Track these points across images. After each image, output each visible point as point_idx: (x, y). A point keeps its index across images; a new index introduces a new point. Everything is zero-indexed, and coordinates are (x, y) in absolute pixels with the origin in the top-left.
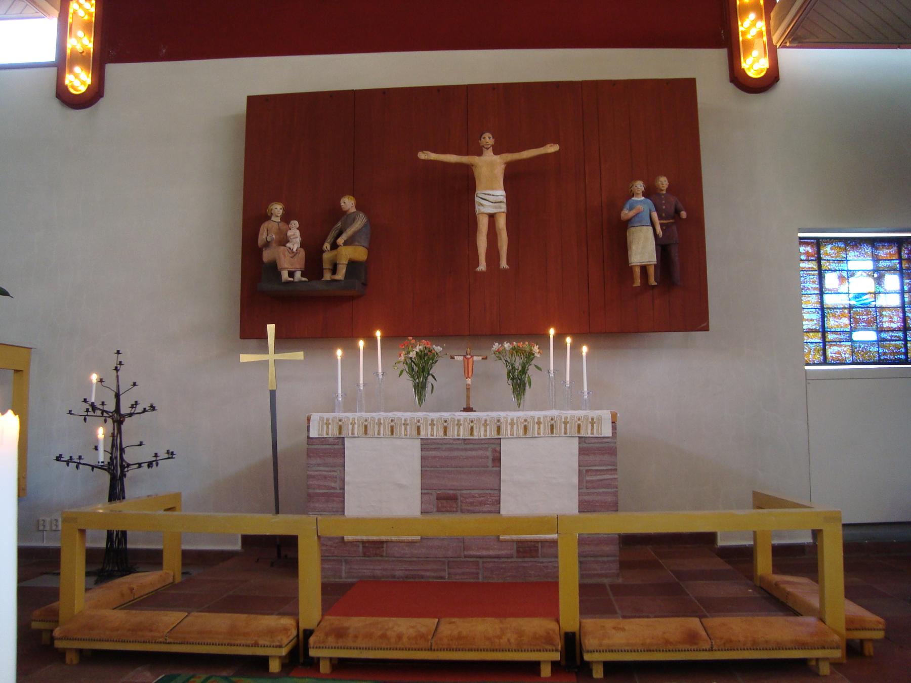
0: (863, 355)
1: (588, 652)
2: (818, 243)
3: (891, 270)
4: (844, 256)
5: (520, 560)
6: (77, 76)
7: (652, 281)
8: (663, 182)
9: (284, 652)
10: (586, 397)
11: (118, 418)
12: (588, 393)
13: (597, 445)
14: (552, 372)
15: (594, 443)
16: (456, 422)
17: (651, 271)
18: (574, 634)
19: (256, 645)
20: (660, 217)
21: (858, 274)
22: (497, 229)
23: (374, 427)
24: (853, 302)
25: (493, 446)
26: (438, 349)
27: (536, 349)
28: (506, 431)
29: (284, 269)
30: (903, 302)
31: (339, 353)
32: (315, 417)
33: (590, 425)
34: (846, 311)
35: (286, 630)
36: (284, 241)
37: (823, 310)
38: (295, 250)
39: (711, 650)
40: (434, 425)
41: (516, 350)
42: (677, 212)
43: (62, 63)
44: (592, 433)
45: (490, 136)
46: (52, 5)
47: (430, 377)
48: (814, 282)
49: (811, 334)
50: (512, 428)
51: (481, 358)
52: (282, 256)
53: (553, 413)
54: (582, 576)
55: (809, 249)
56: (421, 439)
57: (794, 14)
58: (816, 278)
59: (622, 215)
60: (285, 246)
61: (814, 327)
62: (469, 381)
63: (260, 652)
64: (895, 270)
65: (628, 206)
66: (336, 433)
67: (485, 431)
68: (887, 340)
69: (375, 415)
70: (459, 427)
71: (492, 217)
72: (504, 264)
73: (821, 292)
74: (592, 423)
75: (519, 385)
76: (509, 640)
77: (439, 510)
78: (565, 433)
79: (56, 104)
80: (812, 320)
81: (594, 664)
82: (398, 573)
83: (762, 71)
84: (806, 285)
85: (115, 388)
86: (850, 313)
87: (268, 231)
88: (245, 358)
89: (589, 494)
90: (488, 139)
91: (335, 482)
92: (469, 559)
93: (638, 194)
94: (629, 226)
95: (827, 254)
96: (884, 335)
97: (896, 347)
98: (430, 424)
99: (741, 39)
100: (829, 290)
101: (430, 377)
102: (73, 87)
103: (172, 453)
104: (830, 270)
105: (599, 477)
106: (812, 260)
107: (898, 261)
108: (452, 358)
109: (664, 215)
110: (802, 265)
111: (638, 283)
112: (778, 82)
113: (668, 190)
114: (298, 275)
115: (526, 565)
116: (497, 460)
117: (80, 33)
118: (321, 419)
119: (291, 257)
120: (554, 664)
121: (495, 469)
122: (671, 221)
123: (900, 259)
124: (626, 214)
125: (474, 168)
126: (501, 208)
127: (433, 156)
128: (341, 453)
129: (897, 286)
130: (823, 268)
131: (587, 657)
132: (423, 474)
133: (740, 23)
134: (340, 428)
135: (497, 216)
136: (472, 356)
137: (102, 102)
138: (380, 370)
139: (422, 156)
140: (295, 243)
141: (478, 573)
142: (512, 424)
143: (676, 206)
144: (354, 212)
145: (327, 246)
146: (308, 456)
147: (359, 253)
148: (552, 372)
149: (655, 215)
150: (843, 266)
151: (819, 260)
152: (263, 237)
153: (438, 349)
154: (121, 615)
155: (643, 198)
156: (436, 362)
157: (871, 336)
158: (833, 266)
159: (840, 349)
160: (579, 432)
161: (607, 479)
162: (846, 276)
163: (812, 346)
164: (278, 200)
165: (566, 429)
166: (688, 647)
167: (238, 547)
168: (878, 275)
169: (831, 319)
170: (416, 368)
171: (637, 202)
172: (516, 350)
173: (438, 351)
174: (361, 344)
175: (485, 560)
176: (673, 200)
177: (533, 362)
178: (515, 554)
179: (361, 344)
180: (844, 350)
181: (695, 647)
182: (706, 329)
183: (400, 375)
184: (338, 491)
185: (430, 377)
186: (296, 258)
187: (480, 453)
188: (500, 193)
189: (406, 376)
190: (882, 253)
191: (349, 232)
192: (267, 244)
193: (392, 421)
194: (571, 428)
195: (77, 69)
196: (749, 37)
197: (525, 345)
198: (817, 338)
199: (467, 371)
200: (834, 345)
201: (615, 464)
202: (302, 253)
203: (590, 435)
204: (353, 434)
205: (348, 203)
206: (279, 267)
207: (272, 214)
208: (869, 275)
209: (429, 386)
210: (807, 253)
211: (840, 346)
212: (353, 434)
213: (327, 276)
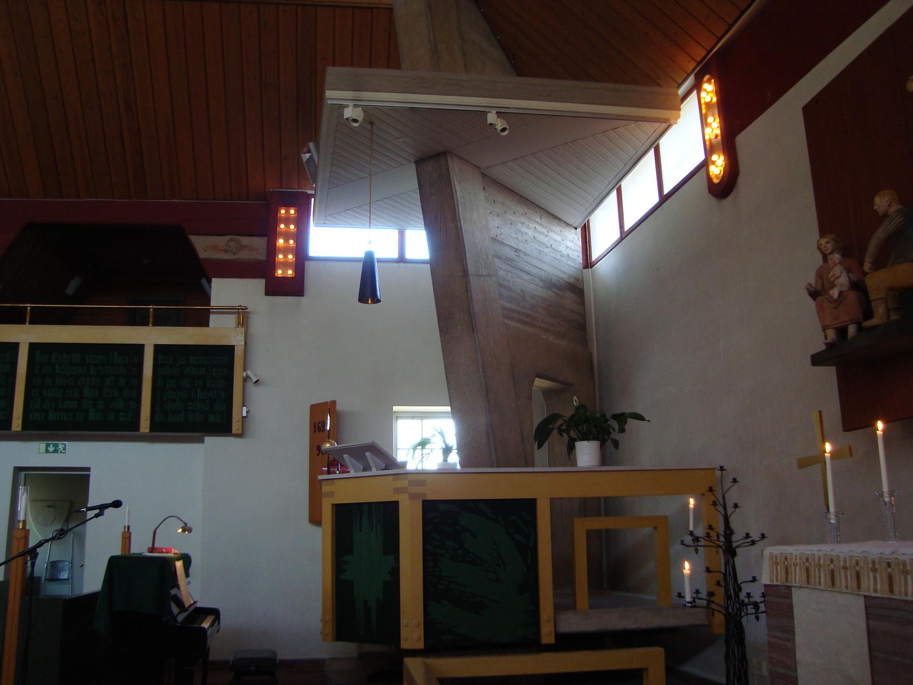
56: (865, 596)
119: (835, 308)
133: (722, 173)
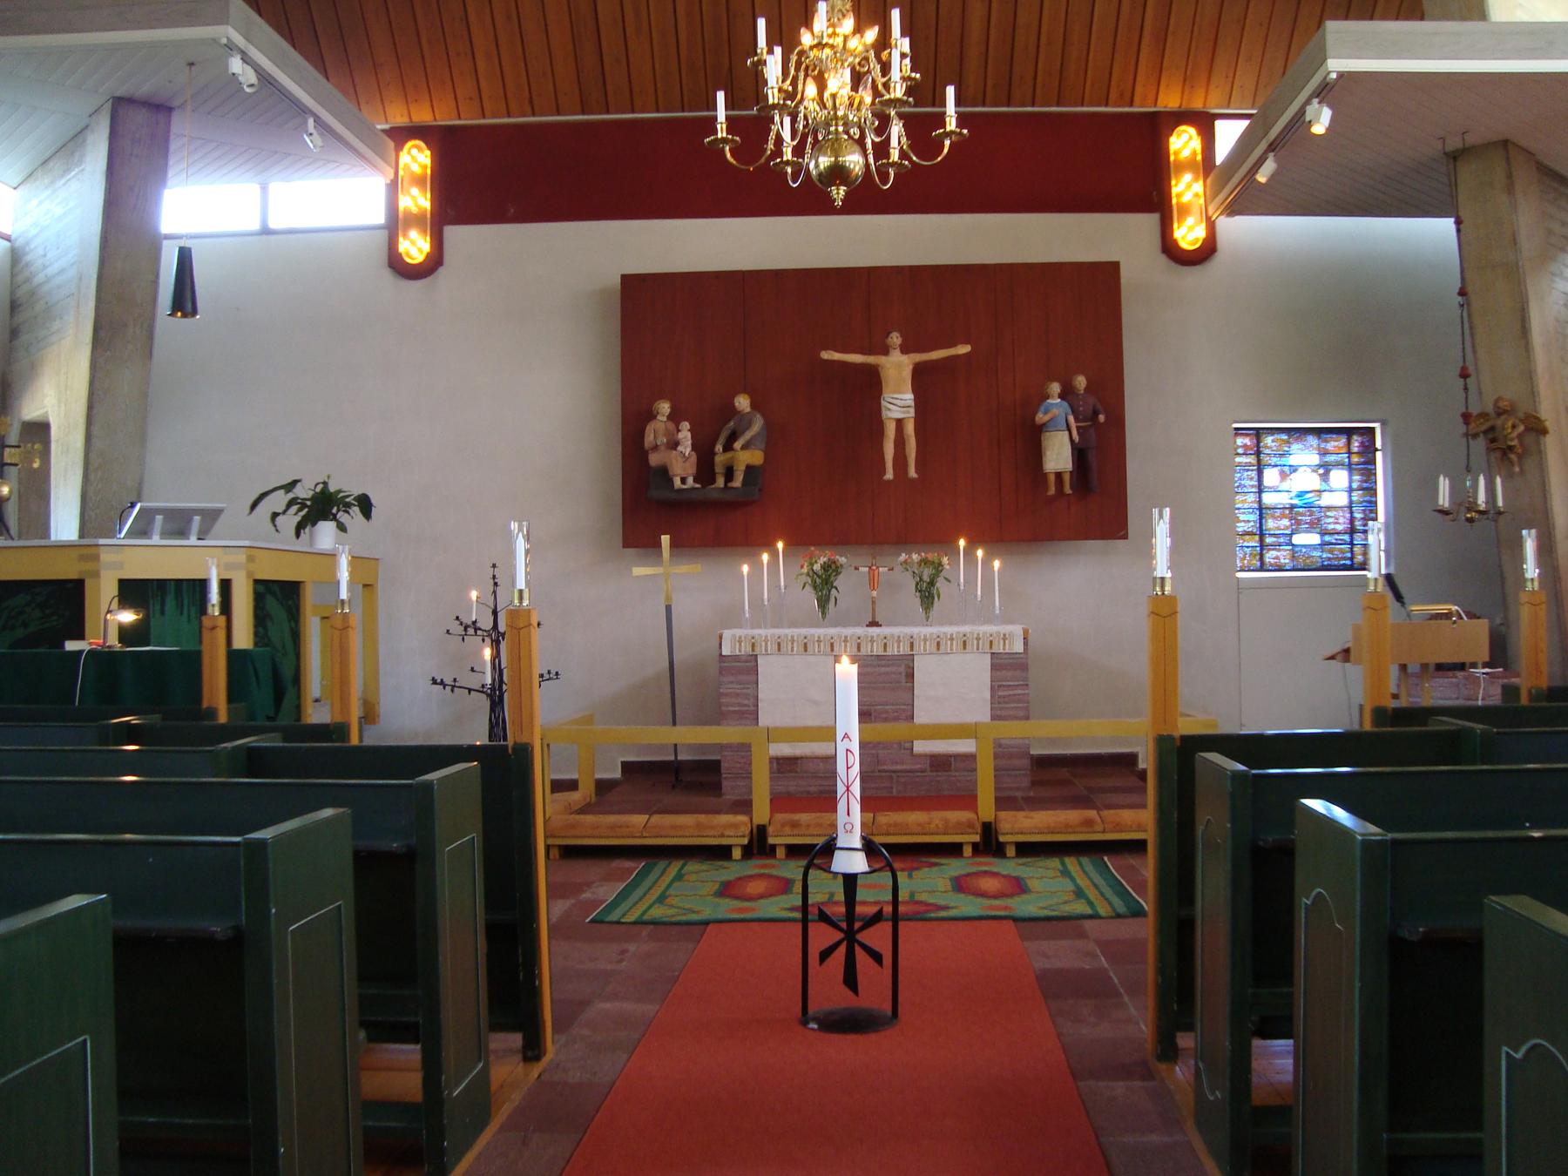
0: (1304, 561)
1: (1003, 834)
2: (1258, 434)
3: (1339, 465)
4: (1286, 449)
5: (935, 774)
6: (413, 243)
7: (1068, 490)
8: (1081, 382)
9: (745, 841)
10: (997, 612)
11: (496, 638)
12: (1000, 609)
13: (1007, 661)
14: (962, 585)
15: (1006, 659)
16: (869, 639)
17: (1067, 478)
18: (990, 823)
19: (722, 836)
20: (1077, 420)
21: (1301, 469)
22: (905, 437)
23: (787, 644)
24: (1295, 501)
25: (906, 662)
26: (842, 560)
27: (945, 560)
29: (677, 475)
30: (1351, 502)
31: (745, 568)
32: (727, 634)
33: (1002, 642)
34: (1287, 512)
36: (674, 445)
37: (1262, 510)
38: (687, 454)
39: (1104, 832)
40: (847, 641)
41: (925, 562)
42: (1096, 413)
43: (395, 224)
44: (1004, 649)
45: (898, 335)
46: (386, 162)
47: (833, 590)
48: (1252, 479)
49: (1247, 537)
50: (925, 644)
51: (886, 569)
52: (674, 461)
53: (966, 629)
54: (996, 789)
55: (1247, 441)
57: (1232, 189)
58: (1254, 474)
59: (1037, 419)
60: (675, 449)
61: (1250, 529)
62: (875, 593)
63: (725, 841)
64: (1343, 465)
65: (1042, 409)
67: (899, 647)
68: (1332, 544)
69: (762, 632)
70: (872, 644)
72: (912, 473)
73: (1260, 490)
74: (1004, 640)
75: (927, 598)
76: (937, 825)
78: (978, 649)
79: (388, 276)
80: (1249, 521)
81: (1008, 846)
82: (813, 789)
83: (1197, 240)
84: (1243, 482)
86: (1290, 513)
87: (655, 432)
88: (638, 571)
89: (1001, 709)
90: (895, 339)
91: (749, 699)
92: (883, 774)
93: (1053, 396)
94: (1044, 430)
95: (1267, 447)
96: (1327, 538)
97: (1342, 551)
98: (844, 641)
99: (1174, 201)
100: (1269, 488)
101: (834, 590)
102: (408, 256)
104: (1270, 465)
105: (1011, 692)
106: (1251, 454)
107: (1347, 455)
108: (857, 569)
109: (1081, 417)
110: (1238, 459)
111: (1052, 491)
112: (1216, 254)
113: (1085, 389)
114: (690, 480)
115: (938, 779)
116: (910, 676)
117: (415, 191)
118: (734, 636)
120: (975, 846)
121: (908, 684)
122: (1089, 423)
123: (1350, 453)
124: (1041, 417)
125: (880, 369)
126: (908, 412)
127: (837, 356)
128: (755, 670)
129: (1345, 484)
130: (1263, 463)
131: (1001, 839)
133: (1173, 182)
134: (753, 645)
135: (906, 420)
136: (878, 568)
137: (441, 270)
138: (782, 584)
139: (826, 355)
140: (686, 447)
141: (892, 788)
142: (925, 640)
143: (1094, 406)
144: (748, 413)
145: (719, 448)
146: (720, 673)
147: (755, 457)
148: (962, 585)
149: (1071, 419)
150: (1284, 461)
151: (1258, 453)
152: (649, 439)
153: (842, 560)
155: (1059, 400)
156: (840, 573)
157: (1314, 539)
158: (1274, 460)
159: (1279, 554)
160: (991, 647)
161: (1019, 695)
162: (1288, 472)
163: (1248, 550)
164: (662, 397)
165: (978, 644)
166: (1084, 829)
167: (617, 774)
168: (1325, 469)
169: (1270, 521)
170: (818, 581)
172: (925, 562)
173: (843, 563)
174: (765, 557)
175: (899, 774)
176: (1092, 400)
177: (942, 574)
178: (928, 769)
179: (765, 557)
180: (1283, 556)
181: (1090, 830)
182: (1125, 537)
183: (803, 588)
184: (752, 708)
185: (833, 590)
186: (688, 464)
187: (894, 669)
188: (908, 397)
190: (1331, 446)
191: (748, 435)
192: (655, 448)
193: (805, 638)
194: (983, 644)
195: (414, 234)
196: (1185, 199)
197: (932, 556)
198: (1254, 542)
199: (873, 582)
200: (1273, 550)
201: (1026, 679)
202: (694, 458)
203: (1001, 651)
204: (766, 650)
205: (743, 403)
206: (671, 473)
207: (658, 413)
208: (1313, 471)
209: (832, 600)
210: (1245, 446)
211: (1279, 550)
212: (766, 650)
213: (720, 482)
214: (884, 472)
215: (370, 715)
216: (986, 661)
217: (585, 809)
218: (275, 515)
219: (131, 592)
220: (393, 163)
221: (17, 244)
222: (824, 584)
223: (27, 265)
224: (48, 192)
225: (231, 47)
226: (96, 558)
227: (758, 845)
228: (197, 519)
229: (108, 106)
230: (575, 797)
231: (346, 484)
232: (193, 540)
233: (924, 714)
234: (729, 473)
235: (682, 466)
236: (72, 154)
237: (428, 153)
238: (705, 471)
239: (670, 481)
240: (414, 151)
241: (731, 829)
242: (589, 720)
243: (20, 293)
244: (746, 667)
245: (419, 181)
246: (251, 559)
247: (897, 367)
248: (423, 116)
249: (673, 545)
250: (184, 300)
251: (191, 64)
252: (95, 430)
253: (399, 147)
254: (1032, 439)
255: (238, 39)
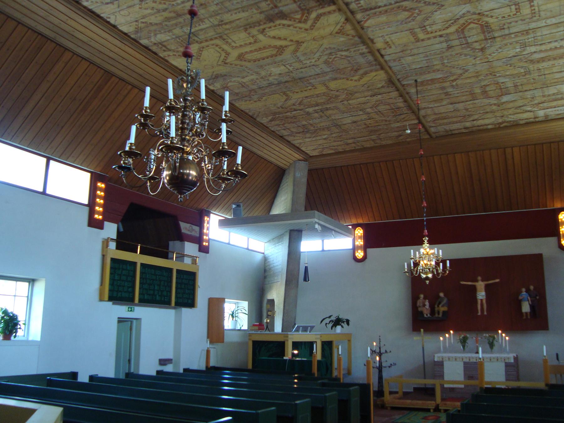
8: (532, 287)
17: (529, 314)
26: (468, 335)
27: (496, 336)
28: (485, 360)
32: (436, 355)
35: (434, 404)
43: (355, 249)
46: (351, 234)
62: (477, 345)
66: (442, 360)
71: (482, 300)
72: (485, 313)
74: (508, 358)
77: (468, 380)
79: (353, 261)
85: (379, 346)
87: (419, 303)
88: (415, 338)
103: (395, 364)
108: (472, 338)
114: (429, 315)
117: (359, 240)
124: (520, 298)
132: (464, 371)
137: (367, 260)
140: (427, 306)
145: (436, 306)
147: (445, 309)
149: (529, 298)
154: (398, 401)
171: (523, 294)
172: (490, 336)
188: (483, 293)
189: (460, 343)
191: (442, 303)
197: (492, 335)
202: (430, 308)
205: (442, 295)
213: (437, 315)
214: (477, 312)
215: (349, 372)
216: (503, 364)
217: (400, 398)
218: (326, 324)
219: (296, 345)
220: (354, 234)
221: (266, 256)
222: (464, 341)
223: (269, 262)
224: (274, 246)
225: (316, 223)
226: (287, 337)
227: (437, 409)
228: (309, 328)
229: (289, 231)
230: (397, 395)
231: (343, 316)
232: (308, 332)
233: (446, 378)
234: (439, 313)
235: (426, 310)
236: (280, 239)
237: (362, 230)
238: (433, 312)
239: (423, 315)
240: (359, 230)
241: (431, 404)
242: (401, 377)
243: (267, 268)
244: (440, 364)
245: (360, 237)
246: (321, 337)
247: (480, 285)
248: (360, 221)
249: (424, 331)
250: (306, 279)
251: (307, 225)
252: (286, 305)
253: (355, 229)
254: (519, 304)
255: (317, 220)
